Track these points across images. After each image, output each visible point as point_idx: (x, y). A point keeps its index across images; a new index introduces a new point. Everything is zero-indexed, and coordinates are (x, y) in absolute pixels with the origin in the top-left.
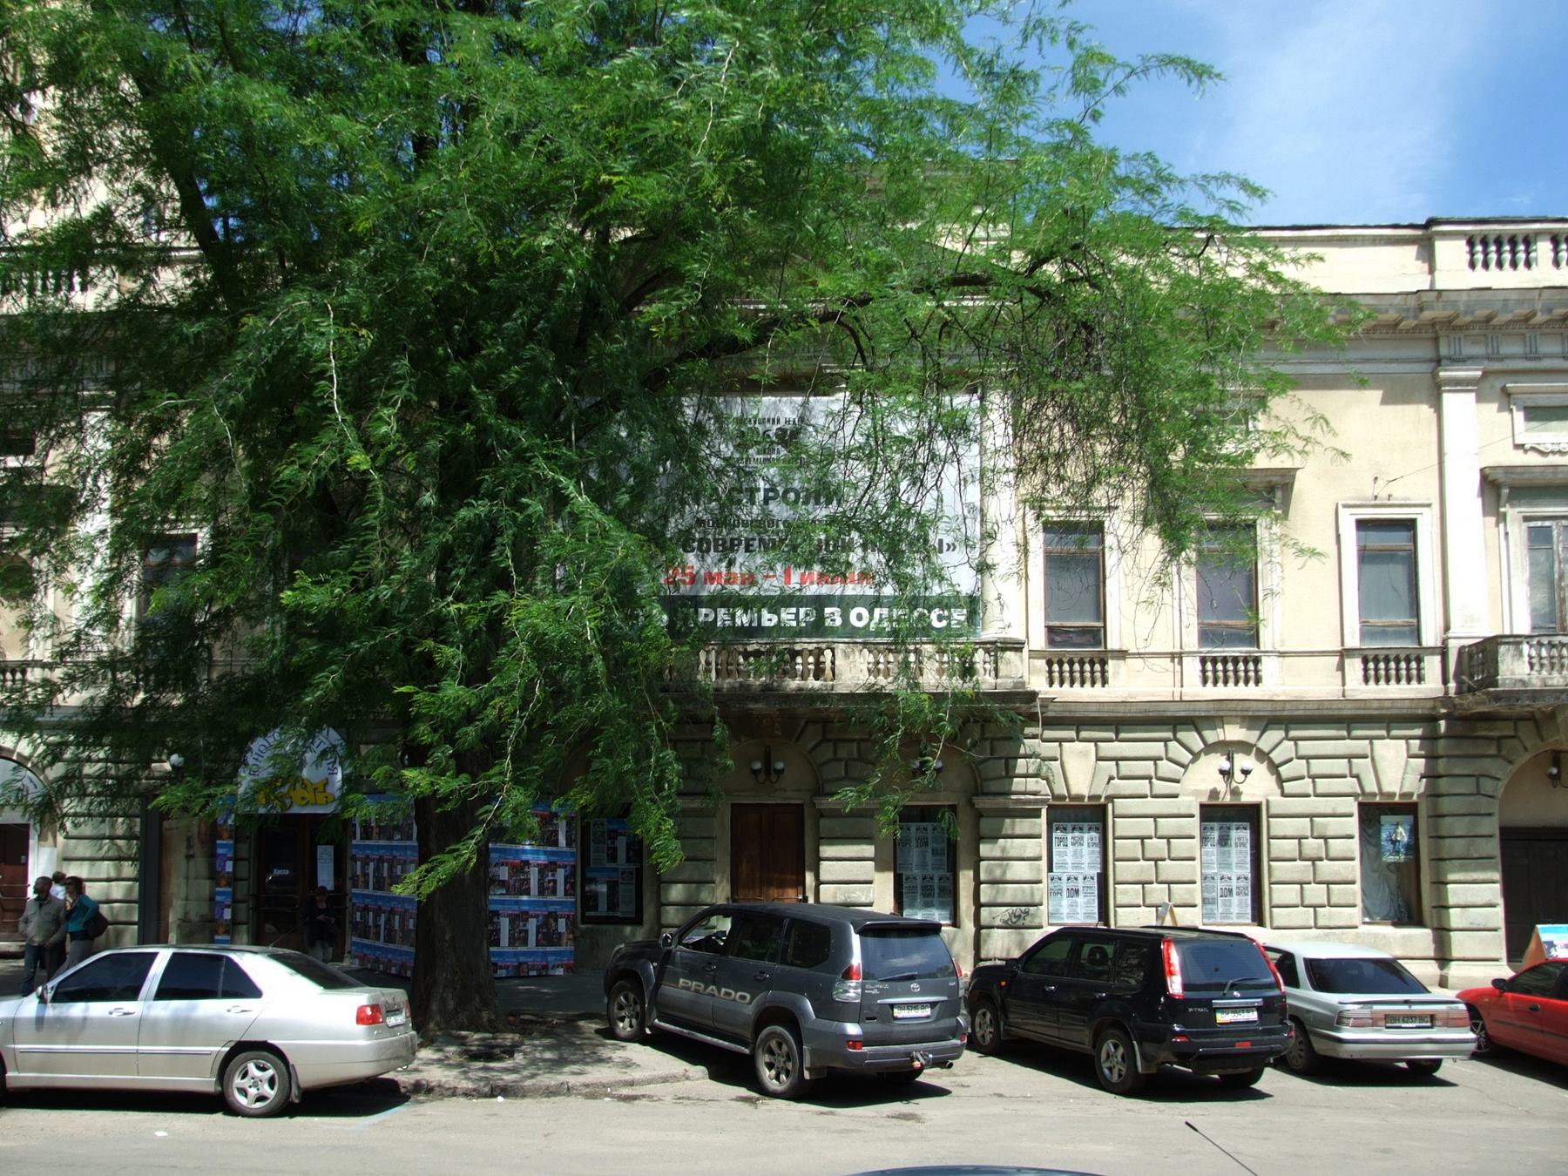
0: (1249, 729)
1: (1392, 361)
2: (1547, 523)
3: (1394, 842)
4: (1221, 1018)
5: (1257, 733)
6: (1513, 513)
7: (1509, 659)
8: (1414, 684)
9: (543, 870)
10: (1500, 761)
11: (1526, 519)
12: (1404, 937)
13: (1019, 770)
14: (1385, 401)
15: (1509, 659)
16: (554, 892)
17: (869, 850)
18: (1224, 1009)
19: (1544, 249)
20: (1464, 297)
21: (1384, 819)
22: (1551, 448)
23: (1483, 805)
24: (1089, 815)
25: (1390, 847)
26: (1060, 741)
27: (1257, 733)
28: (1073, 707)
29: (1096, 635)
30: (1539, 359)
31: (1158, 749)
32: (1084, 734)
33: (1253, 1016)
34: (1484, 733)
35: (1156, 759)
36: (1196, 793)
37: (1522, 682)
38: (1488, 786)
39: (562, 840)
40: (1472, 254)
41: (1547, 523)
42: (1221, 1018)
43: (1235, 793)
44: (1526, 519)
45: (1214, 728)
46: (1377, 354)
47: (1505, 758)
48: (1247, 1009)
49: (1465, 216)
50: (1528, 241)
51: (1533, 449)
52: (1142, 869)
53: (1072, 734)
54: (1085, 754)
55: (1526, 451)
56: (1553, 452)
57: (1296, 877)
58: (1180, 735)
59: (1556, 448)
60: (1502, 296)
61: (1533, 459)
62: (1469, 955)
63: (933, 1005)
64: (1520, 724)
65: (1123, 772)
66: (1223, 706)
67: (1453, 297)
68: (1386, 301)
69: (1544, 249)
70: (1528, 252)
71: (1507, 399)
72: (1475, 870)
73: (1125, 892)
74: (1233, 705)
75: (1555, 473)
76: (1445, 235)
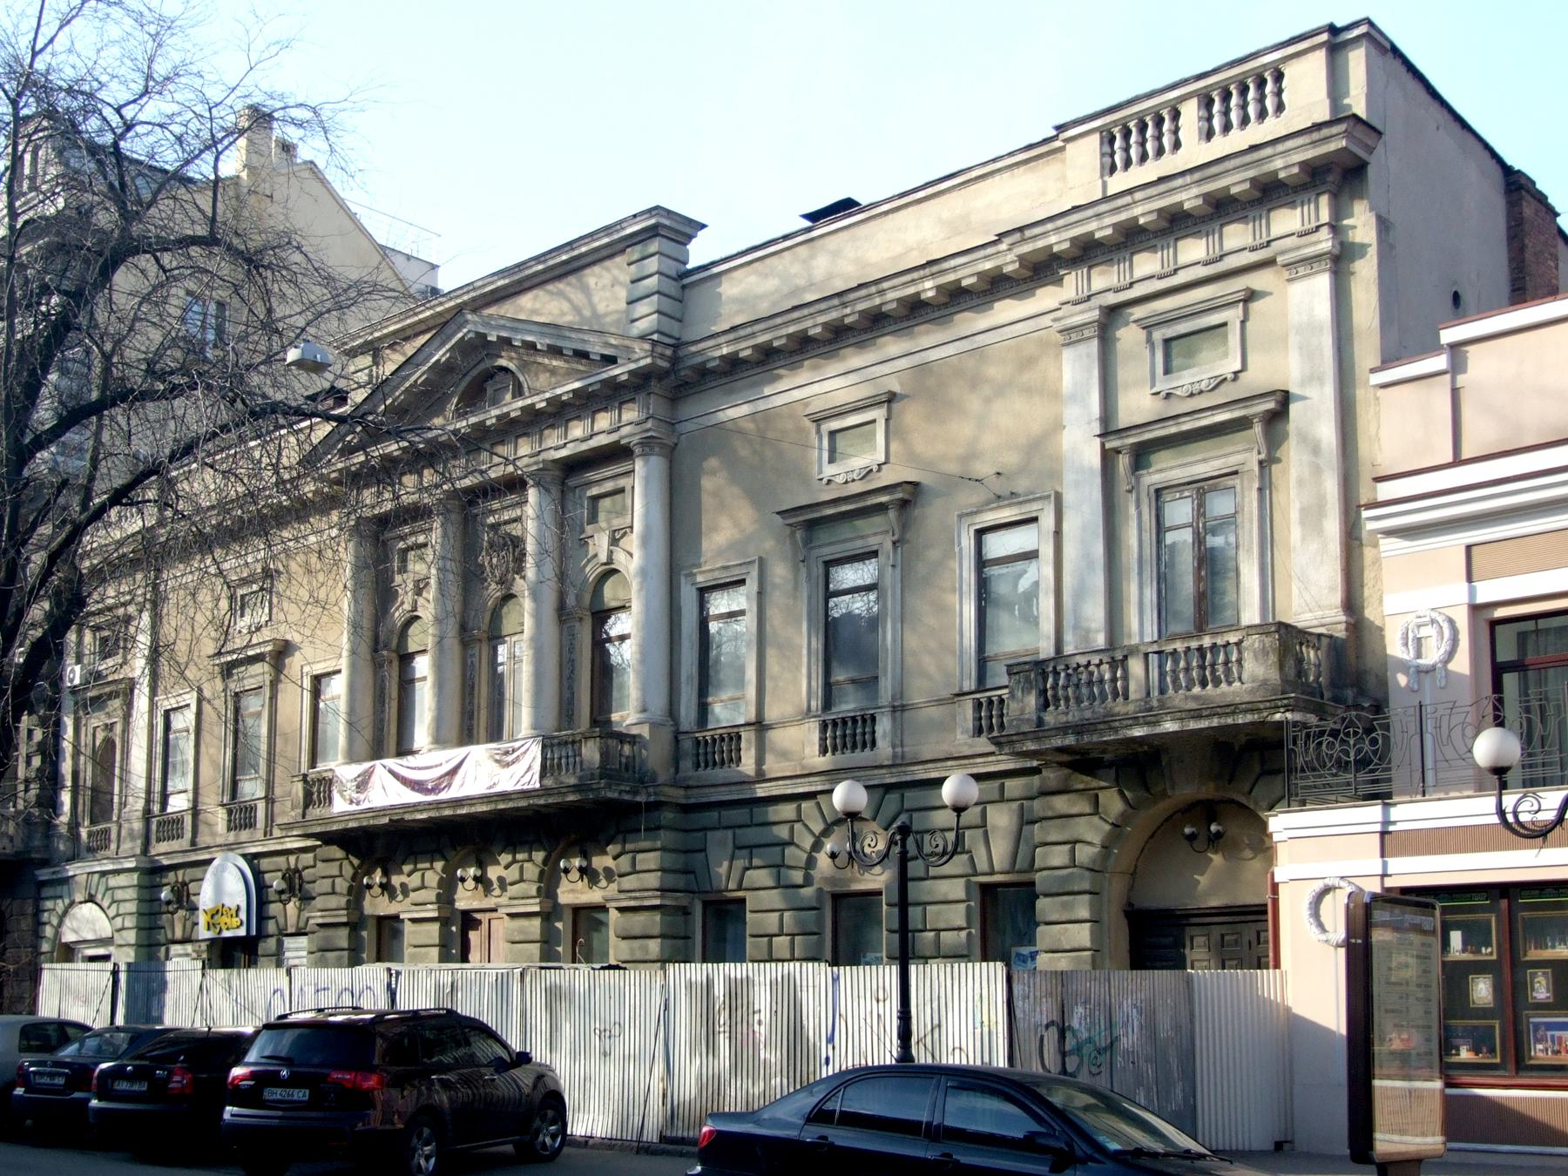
8: (717, 770)
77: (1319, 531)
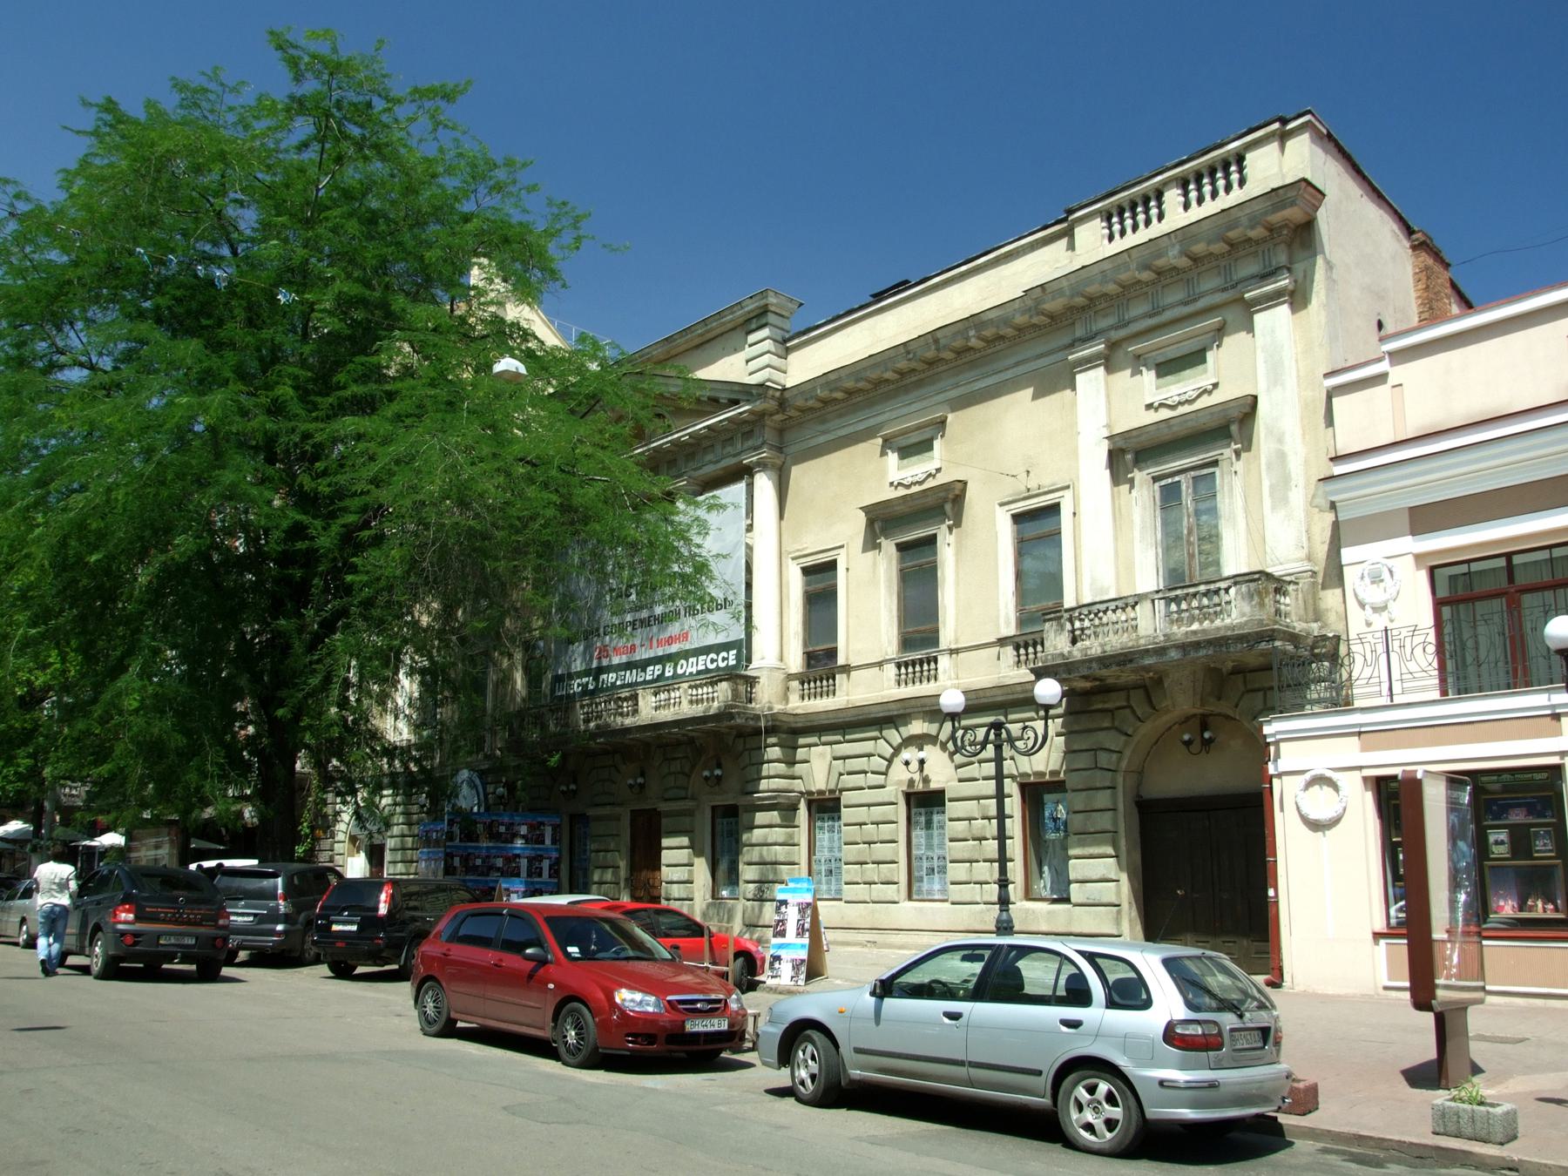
0: (931, 722)
1: (1017, 364)
2: (1177, 479)
3: (1055, 820)
4: (335, 927)
5: (936, 725)
6: (1140, 476)
7: (1052, 635)
8: (812, 701)
9: (531, 860)
10: (1113, 732)
11: (1155, 479)
12: (1049, 912)
13: (764, 773)
14: (1035, 397)
15: (1052, 635)
16: (540, 875)
17: (685, 841)
18: (338, 922)
19: (1173, 197)
20: (1065, 283)
21: (1047, 797)
22: (1177, 399)
23: (1102, 779)
24: (826, 806)
25: (1050, 824)
26: (809, 746)
27: (936, 725)
28: (866, 710)
29: (832, 653)
30: (1195, 300)
31: (867, 747)
32: (824, 739)
33: (354, 928)
34: (1100, 706)
35: (869, 755)
36: (899, 783)
37: (1062, 655)
38: (1104, 760)
39: (548, 841)
40: (1110, 227)
41: (1177, 479)
42: (335, 927)
43: (926, 780)
44: (1155, 479)
45: (906, 724)
46: (1029, 354)
47: (1117, 729)
48: (351, 923)
49: (1092, 198)
50: (1159, 195)
51: (1162, 405)
52: (859, 851)
53: (839, 738)
54: (822, 755)
55: (1156, 409)
56: (1180, 403)
57: (966, 856)
58: (885, 733)
59: (1183, 398)
60: (1096, 270)
61: (1165, 414)
62: (1086, 930)
63: (255, 915)
64: (1132, 693)
65: (849, 769)
66: (906, 704)
67: (1055, 286)
68: (1009, 309)
69: (1173, 197)
70: (1159, 206)
71: (1138, 363)
72: (1090, 845)
73: (848, 871)
74: (913, 702)
75: (1169, 427)
76: (1082, 220)
77: (1284, 500)
